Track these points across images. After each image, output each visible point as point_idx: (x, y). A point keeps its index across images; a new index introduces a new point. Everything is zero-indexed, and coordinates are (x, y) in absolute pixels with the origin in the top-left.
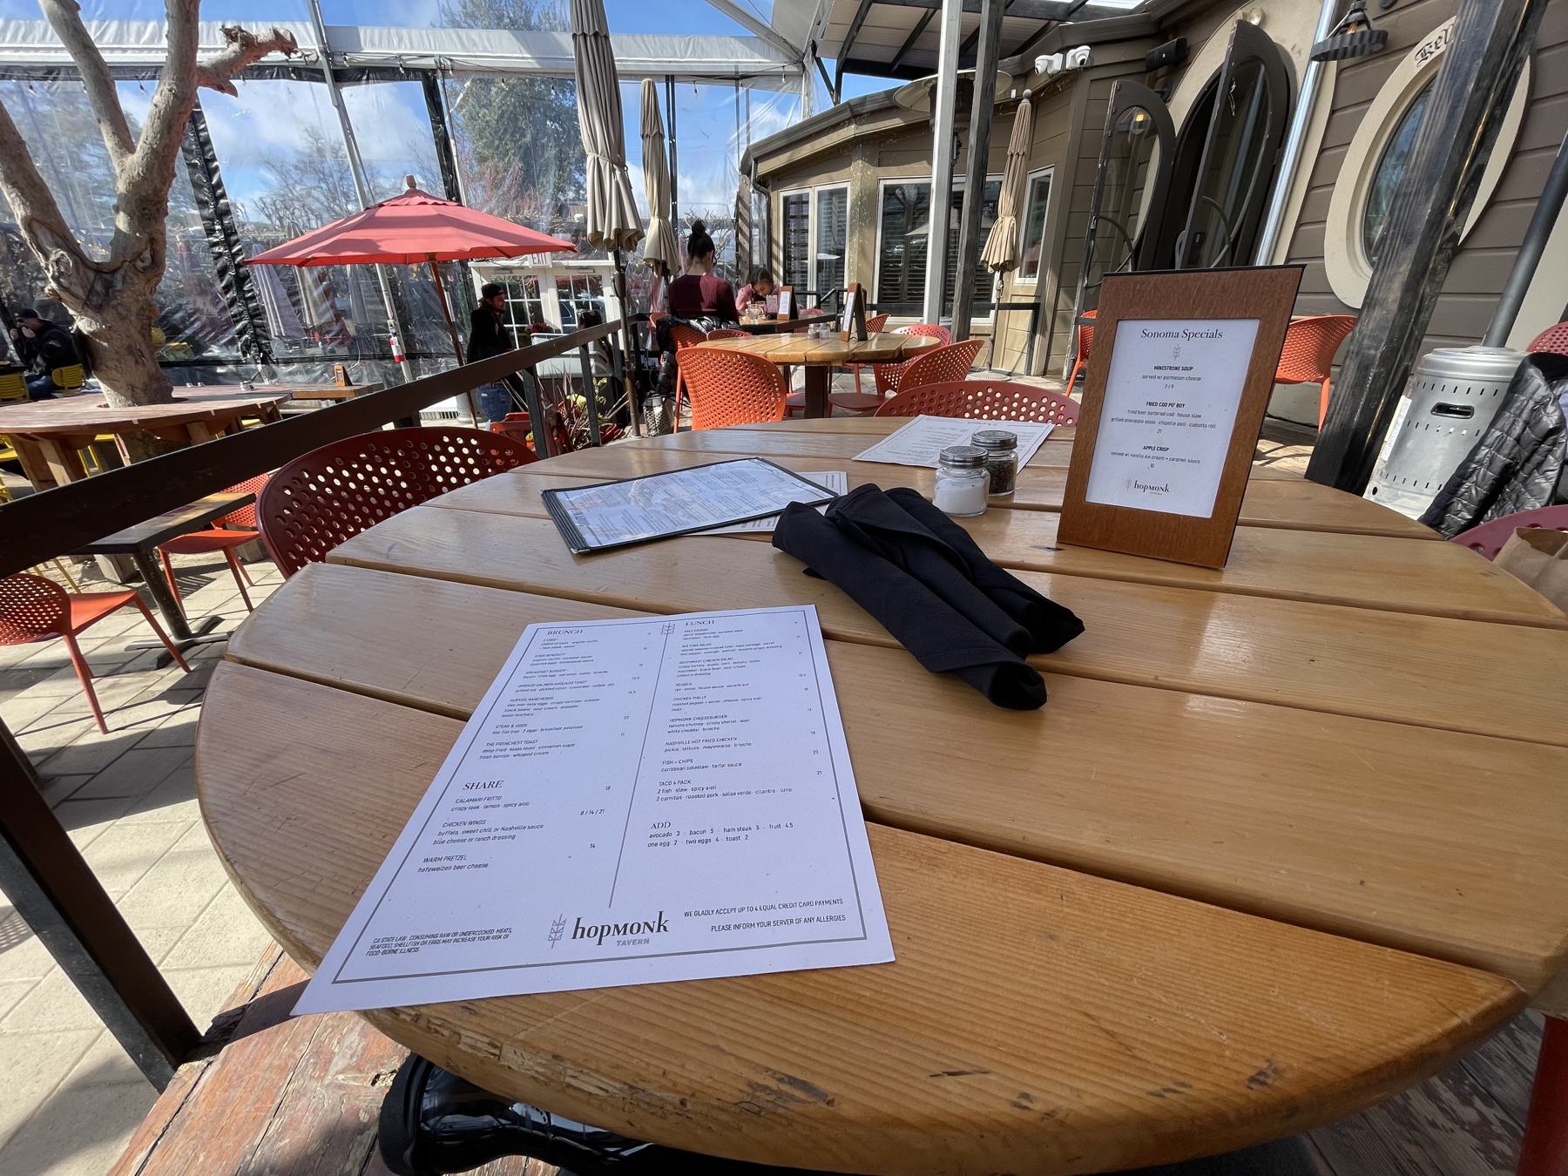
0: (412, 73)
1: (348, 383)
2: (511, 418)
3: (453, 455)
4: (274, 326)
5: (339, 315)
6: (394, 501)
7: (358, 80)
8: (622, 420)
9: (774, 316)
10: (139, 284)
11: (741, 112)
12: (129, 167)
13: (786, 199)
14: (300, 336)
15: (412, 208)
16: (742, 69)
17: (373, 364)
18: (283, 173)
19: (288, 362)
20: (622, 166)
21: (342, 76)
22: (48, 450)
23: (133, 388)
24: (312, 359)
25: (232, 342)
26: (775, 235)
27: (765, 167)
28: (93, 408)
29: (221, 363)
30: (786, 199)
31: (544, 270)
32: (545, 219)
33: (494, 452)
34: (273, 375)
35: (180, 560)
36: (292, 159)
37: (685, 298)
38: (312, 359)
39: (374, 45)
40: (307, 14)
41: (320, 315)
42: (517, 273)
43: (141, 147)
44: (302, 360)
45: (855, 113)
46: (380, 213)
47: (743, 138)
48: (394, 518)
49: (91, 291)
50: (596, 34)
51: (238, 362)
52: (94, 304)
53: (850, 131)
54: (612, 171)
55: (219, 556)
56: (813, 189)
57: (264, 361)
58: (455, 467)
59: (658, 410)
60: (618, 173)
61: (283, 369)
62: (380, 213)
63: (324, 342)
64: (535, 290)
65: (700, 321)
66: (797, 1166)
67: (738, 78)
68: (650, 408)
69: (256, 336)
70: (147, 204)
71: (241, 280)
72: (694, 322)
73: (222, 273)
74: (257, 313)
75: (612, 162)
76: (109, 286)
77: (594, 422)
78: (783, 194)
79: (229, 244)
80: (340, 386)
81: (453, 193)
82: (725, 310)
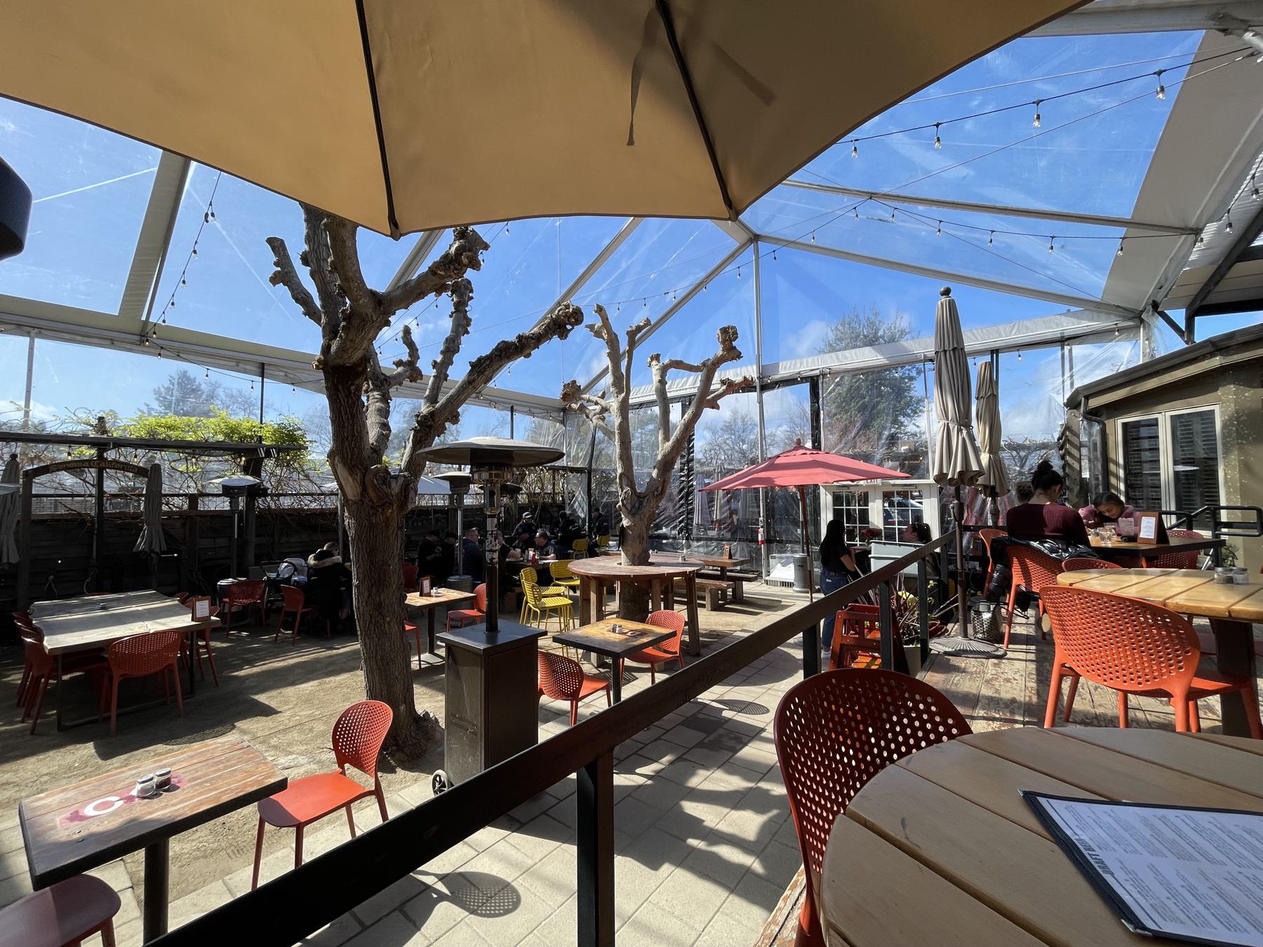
0: (804, 379)
1: (730, 557)
2: (852, 609)
3: (915, 719)
4: (696, 519)
5: (733, 512)
6: (884, 760)
7: (773, 388)
8: (947, 618)
9: (1133, 538)
10: (653, 503)
11: (1067, 363)
12: (664, 447)
13: (1125, 425)
14: (709, 523)
15: (797, 457)
16: (1067, 334)
17: (744, 544)
18: (714, 433)
19: (698, 540)
20: (968, 426)
21: (765, 387)
22: (593, 585)
23: (634, 555)
24: (711, 539)
25: (675, 527)
26: (1112, 455)
27: (1094, 403)
28: (615, 564)
29: (666, 537)
30: (1125, 425)
31: (875, 487)
32: (880, 453)
33: (917, 697)
34: (689, 547)
35: (628, 662)
36: (721, 425)
37: (1025, 523)
38: (711, 539)
39: (785, 370)
40: (755, 361)
41: (721, 513)
42: (852, 489)
43: (673, 439)
44: (706, 539)
45: (1217, 346)
46: (778, 461)
47: (1068, 383)
48: (881, 773)
49: (633, 507)
50: (954, 349)
51: (675, 538)
52: (632, 514)
53: (1217, 362)
54: (960, 431)
55: (648, 666)
56: (1164, 417)
57: (687, 539)
58: (915, 730)
59: (987, 616)
60: (964, 432)
61: (695, 544)
62: (778, 461)
63: (720, 529)
64: (865, 499)
65: (1042, 543)
66: (63, 750)
67: (1063, 341)
68: (979, 613)
69: (687, 524)
70: (666, 465)
71: (688, 494)
72: (1035, 544)
73: (681, 491)
74: (691, 512)
75: (960, 425)
76: (641, 503)
77: (923, 619)
78: (1120, 421)
79: (688, 476)
80: (725, 559)
81: (817, 445)
82: (1072, 532)
